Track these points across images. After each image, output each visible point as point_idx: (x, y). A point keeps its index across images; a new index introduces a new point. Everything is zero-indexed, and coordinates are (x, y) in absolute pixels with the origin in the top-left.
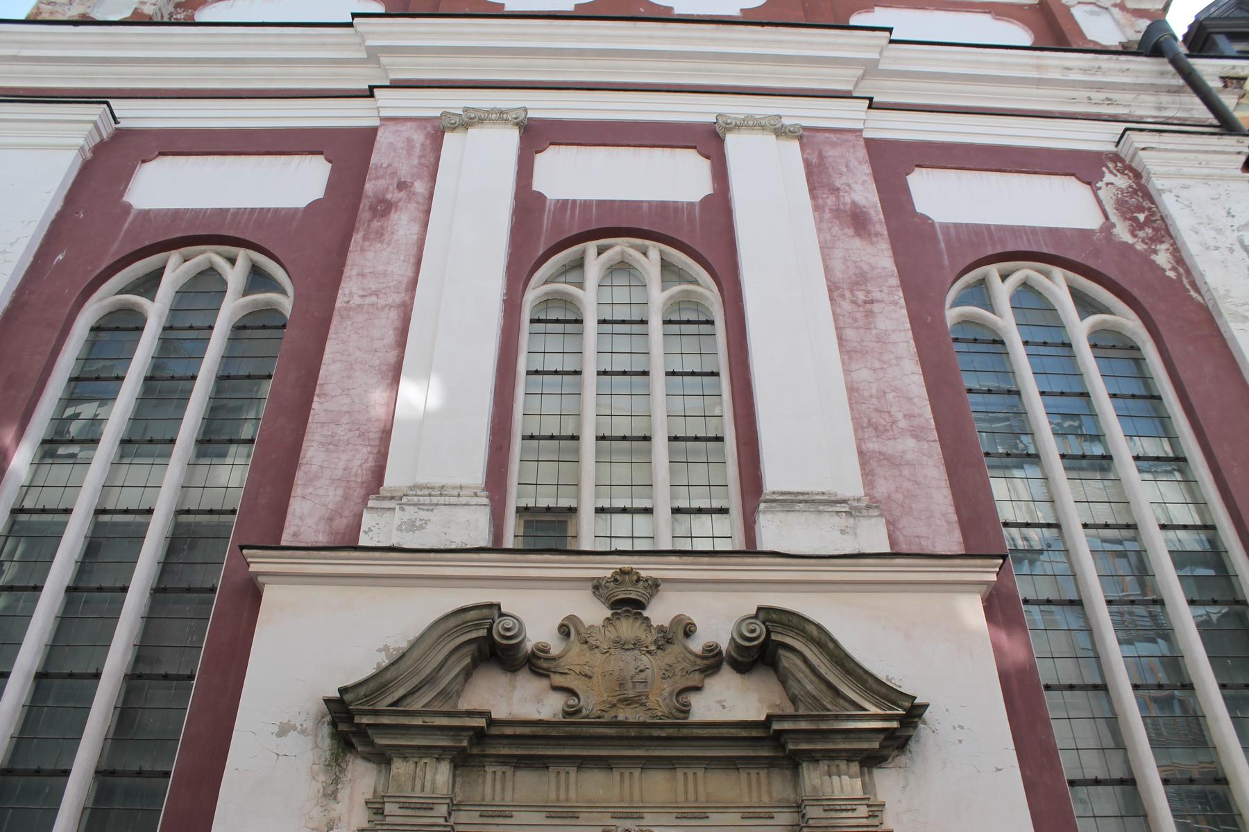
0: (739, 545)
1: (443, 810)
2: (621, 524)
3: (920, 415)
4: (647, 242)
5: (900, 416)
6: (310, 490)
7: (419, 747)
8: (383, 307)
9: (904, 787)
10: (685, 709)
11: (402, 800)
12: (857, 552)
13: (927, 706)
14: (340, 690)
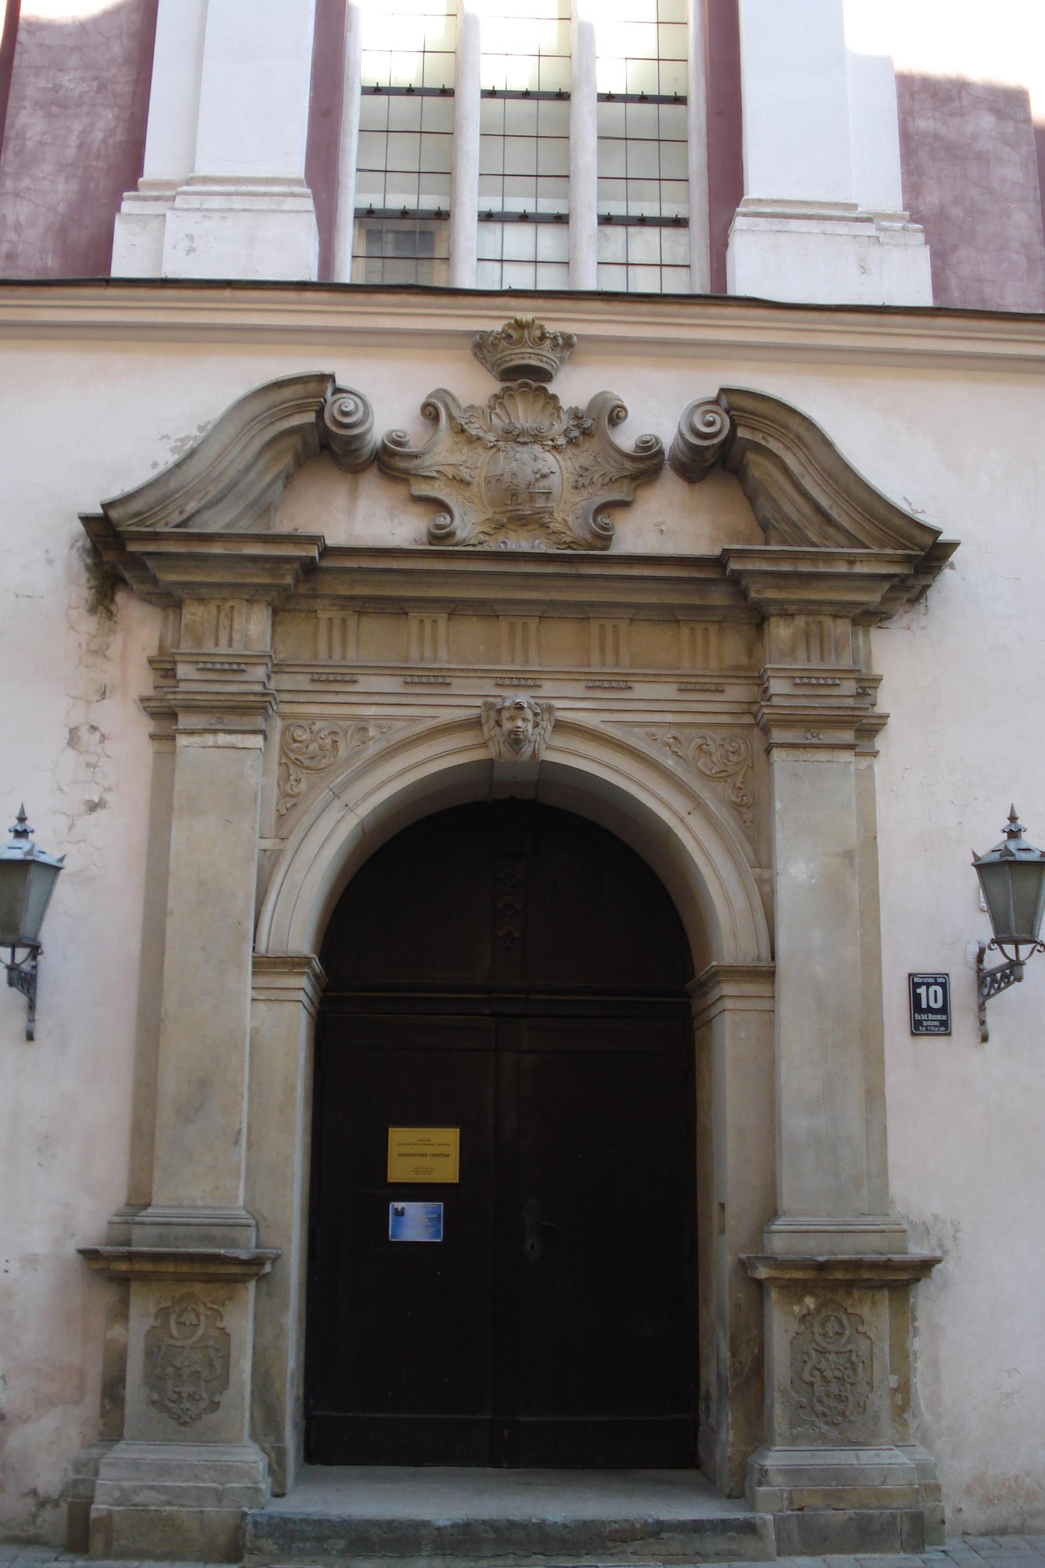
0: (701, 285)
1: (260, 672)
6: (26, 182)
7: (221, 586)
10: (604, 538)
11: (201, 659)
13: (959, 544)
14: (103, 506)
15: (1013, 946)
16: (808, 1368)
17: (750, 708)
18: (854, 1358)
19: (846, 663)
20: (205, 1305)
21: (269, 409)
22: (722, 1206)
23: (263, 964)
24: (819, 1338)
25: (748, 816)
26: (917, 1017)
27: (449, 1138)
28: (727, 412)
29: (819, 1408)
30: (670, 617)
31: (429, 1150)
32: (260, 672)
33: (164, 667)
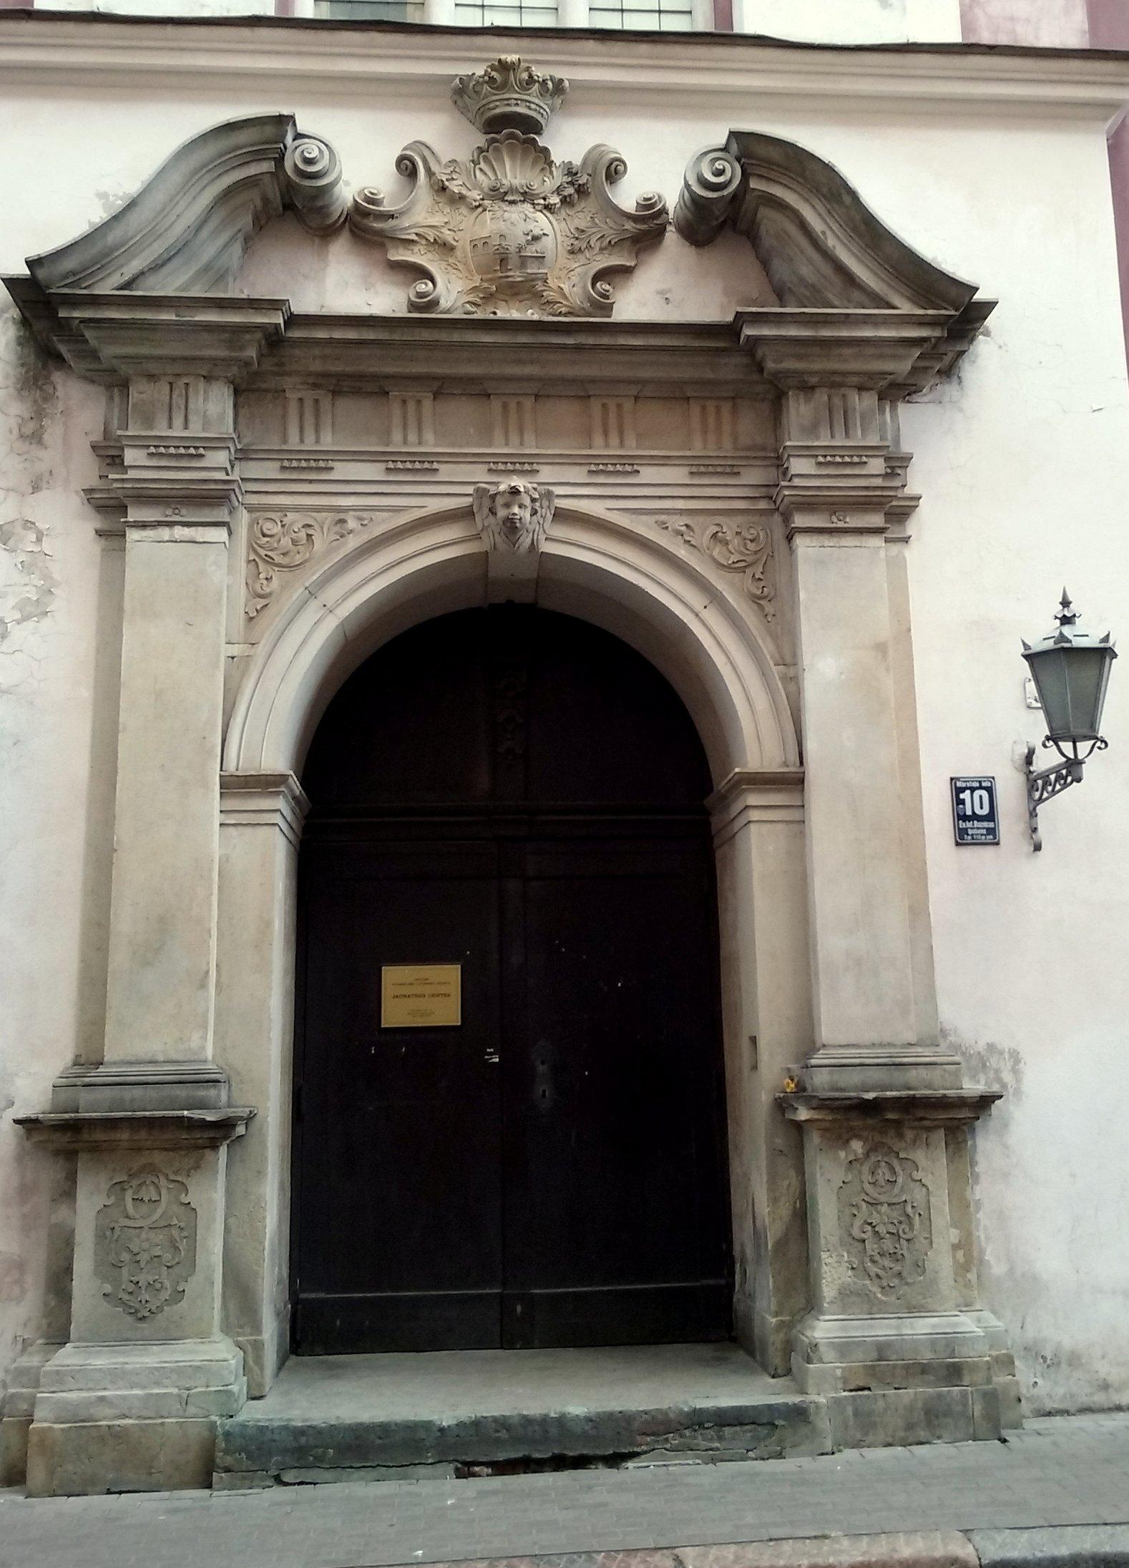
12: (902, 40)
14: (30, 263)
15: (1071, 744)
16: (858, 1222)
17: (769, 491)
18: (909, 1210)
19: (873, 441)
20: (167, 1176)
21: (221, 156)
22: (753, 1040)
23: (234, 785)
24: (867, 1187)
25: (769, 608)
26: (962, 825)
27: (448, 976)
28: (738, 160)
29: (873, 1269)
30: (677, 394)
31: (428, 990)
32: (221, 458)
33: (109, 454)
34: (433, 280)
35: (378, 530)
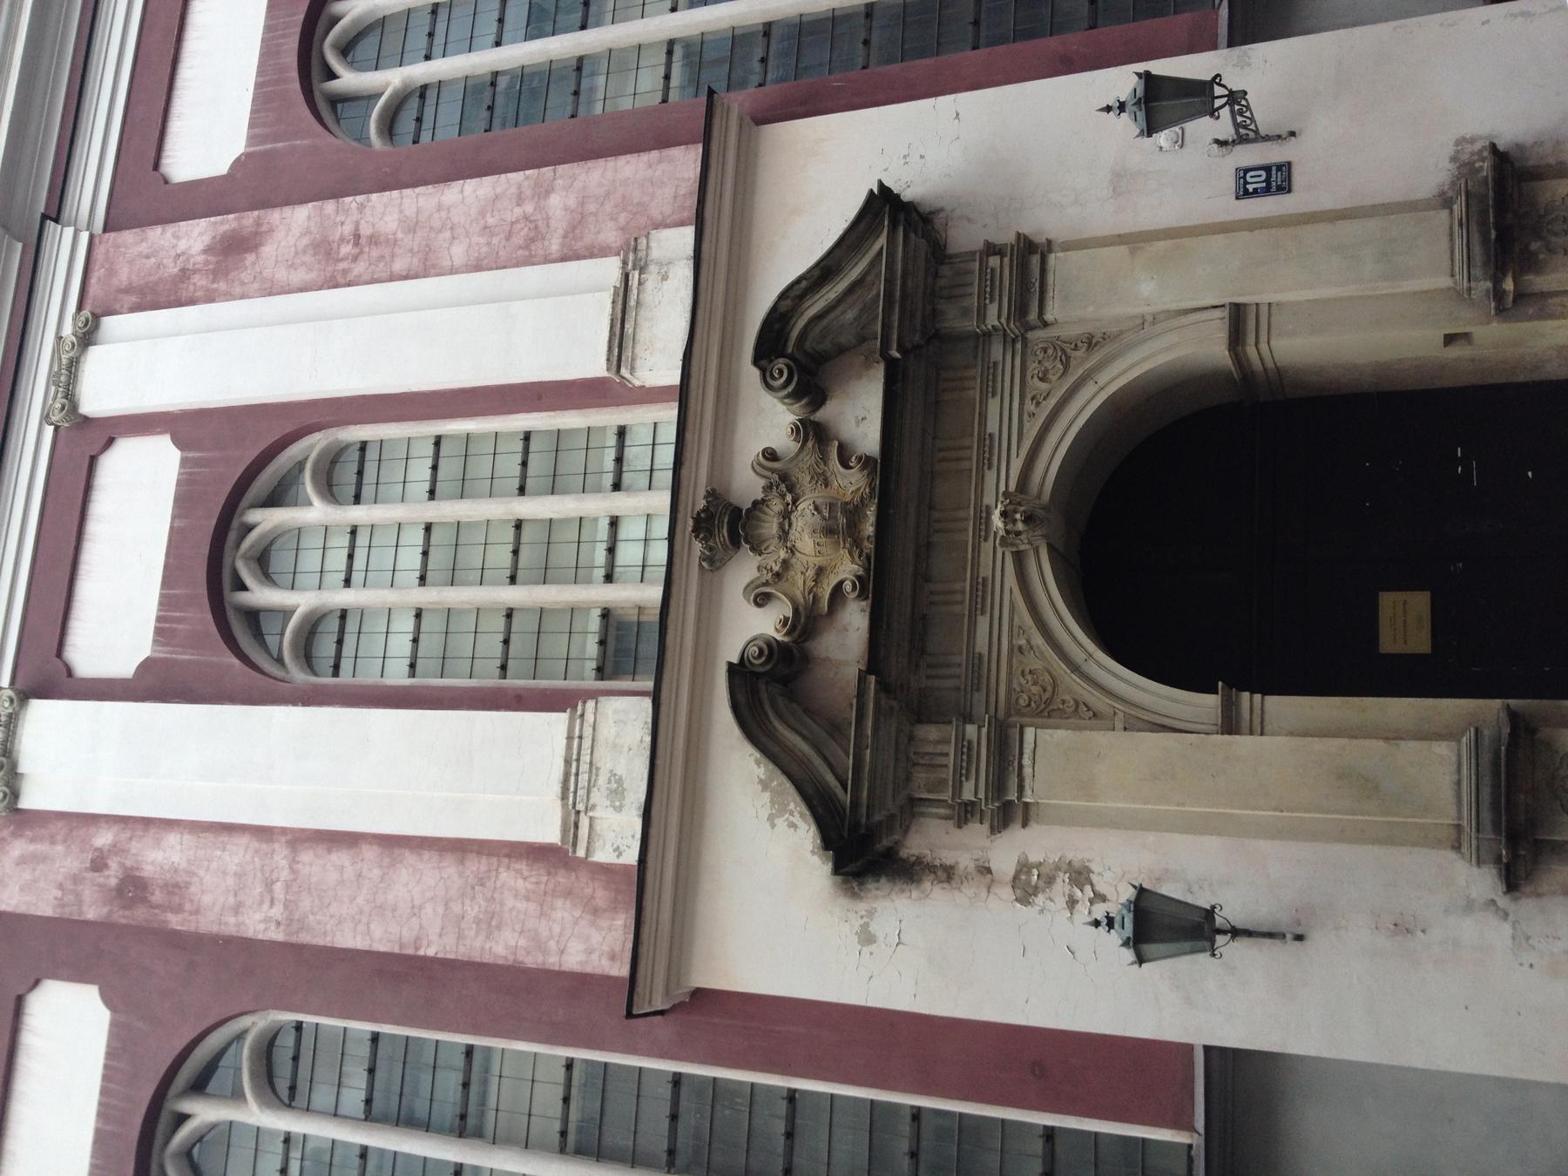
2: (629, 554)
3: (519, 186)
4: (235, 524)
5: (518, 211)
6: (552, 944)
8: (293, 871)
9: (969, 220)
17: (1009, 342)
33: (965, 813)
34: (841, 583)
35: (1029, 621)
